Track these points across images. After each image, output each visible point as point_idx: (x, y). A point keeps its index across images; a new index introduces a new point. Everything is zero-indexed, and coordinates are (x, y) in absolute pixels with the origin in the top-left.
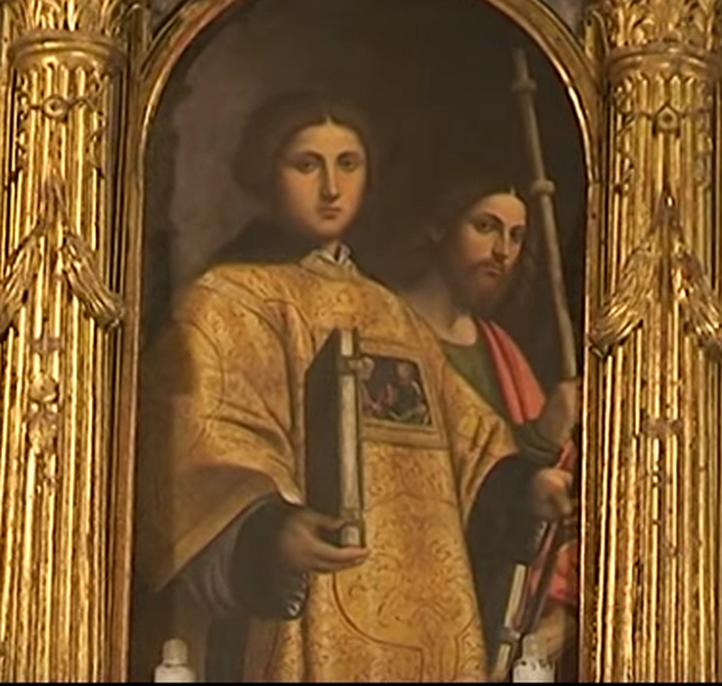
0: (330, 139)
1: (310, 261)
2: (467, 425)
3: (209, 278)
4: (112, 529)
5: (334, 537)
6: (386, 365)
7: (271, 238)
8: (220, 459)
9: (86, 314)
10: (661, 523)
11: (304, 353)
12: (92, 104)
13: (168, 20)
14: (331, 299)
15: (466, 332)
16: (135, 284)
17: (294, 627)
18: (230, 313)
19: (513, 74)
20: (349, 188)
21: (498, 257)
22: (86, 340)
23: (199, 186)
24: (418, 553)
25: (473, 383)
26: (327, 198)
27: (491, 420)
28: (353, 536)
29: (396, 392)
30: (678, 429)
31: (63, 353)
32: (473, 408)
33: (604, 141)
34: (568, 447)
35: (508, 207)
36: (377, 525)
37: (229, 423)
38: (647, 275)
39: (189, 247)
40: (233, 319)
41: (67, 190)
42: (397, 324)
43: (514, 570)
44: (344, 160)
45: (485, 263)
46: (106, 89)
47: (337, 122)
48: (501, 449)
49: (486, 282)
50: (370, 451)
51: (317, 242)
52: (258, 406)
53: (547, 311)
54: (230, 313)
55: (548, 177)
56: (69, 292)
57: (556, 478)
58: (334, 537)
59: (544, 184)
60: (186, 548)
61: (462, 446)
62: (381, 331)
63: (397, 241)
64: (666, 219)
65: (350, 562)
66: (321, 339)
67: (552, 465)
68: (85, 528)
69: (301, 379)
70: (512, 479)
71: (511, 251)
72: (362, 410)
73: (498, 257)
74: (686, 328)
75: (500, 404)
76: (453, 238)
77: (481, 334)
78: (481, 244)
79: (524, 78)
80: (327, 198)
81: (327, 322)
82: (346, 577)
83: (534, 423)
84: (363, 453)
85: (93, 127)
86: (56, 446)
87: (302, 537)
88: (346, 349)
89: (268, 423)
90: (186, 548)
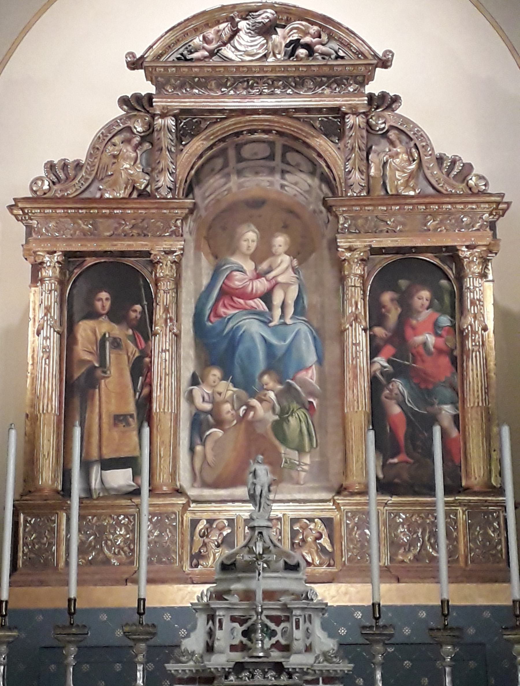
0: (104, 295)
1: (101, 319)
2: (130, 350)
3: (81, 323)
4: (61, 373)
5: (105, 372)
6: (115, 339)
7: (92, 314)
8: (83, 358)
9: (54, 331)
10: (165, 369)
11: (99, 337)
12: (55, 290)
13: (71, 273)
14: (105, 327)
15: (130, 332)
16: (65, 324)
17: (97, 390)
18: (85, 329)
19: (139, 280)
20: (108, 304)
21: (136, 317)
22: (55, 337)
23: (77, 307)
24: (121, 375)
25: (132, 342)
26: (103, 306)
27: (135, 349)
28: (108, 372)
29: (117, 344)
30: (168, 351)
31: (50, 339)
32: (132, 347)
33: (156, 294)
34: (150, 354)
35: (138, 307)
36: (113, 371)
37: (84, 351)
38: (162, 321)
39: (76, 317)
40: (85, 330)
41: (50, 306)
42: (117, 331)
43: (139, 378)
44: (107, 299)
45: (134, 319)
46: (58, 287)
47: (106, 292)
48: (137, 355)
49: (134, 322)
50: (112, 355)
51: (101, 315)
52: (90, 347)
53: (144, 329)
54: (85, 329)
55: (146, 301)
56: (51, 327)
57: (147, 360)
58: (105, 372)
59: (145, 303)
60: (76, 375)
61: (129, 354)
62: (114, 332)
63: (117, 315)
64: (166, 310)
65: (108, 377)
66: (103, 334)
67: (147, 357)
68: (54, 373)
69: (98, 342)
70: (140, 359)
71: (139, 316)
72: (110, 348)
73: (136, 317)
74: (170, 331)
75: (137, 346)
76: (128, 312)
77: (134, 333)
78: (133, 315)
79: (141, 282)
80: (103, 306)
81: (103, 331)
82: (107, 380)
83: (143, 349)
84: (110, 356)
85: (17, 435)
86: (48, 358)
87: (99, 373)
88: (107, 336)
89: (92, 351)
90: (76, 375)
